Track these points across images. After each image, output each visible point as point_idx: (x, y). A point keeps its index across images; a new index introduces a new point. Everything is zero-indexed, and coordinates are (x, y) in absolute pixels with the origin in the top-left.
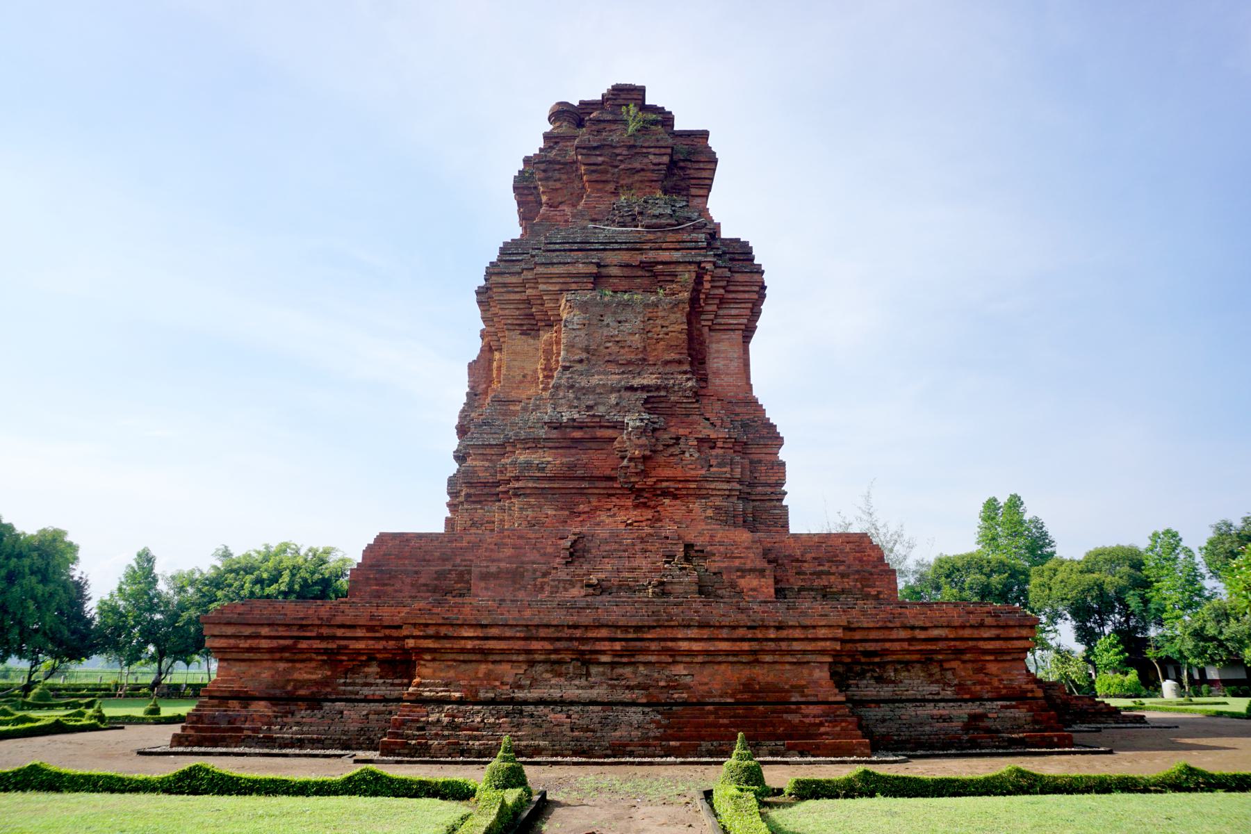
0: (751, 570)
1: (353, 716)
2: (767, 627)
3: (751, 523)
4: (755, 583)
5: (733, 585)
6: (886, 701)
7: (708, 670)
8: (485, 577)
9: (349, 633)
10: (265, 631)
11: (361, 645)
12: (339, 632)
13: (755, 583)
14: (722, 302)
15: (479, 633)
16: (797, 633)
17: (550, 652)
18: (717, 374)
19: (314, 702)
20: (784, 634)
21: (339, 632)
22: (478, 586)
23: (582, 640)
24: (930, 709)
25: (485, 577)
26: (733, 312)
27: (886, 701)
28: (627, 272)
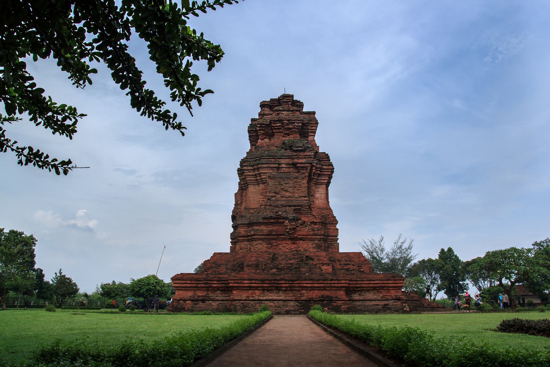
0: (326, 264)
1: (215, 304)
2: (328, 280)
3: (326, 249)
4: (326, 268)
5: (320, 268)
6: (362, 300)
7: (312, 292)
8: (248, 266)
9: (212, 282)
10: (188, 282)
11: (215, 285)
12: (209, 282)
13: (326, 268)
14: (319, 175)
15: (249, 282)
16: (336, 282)
17: (268, 287)
18: (317, 199)
19: (203, 301)
20: (332, 282)
21: (209, 282)
22: (246, 269)
23: (277, 284)
24: (373, 303)
25: (248, 266)
26: (323, 178)
27: (362, 300)
28: (288, 166)
